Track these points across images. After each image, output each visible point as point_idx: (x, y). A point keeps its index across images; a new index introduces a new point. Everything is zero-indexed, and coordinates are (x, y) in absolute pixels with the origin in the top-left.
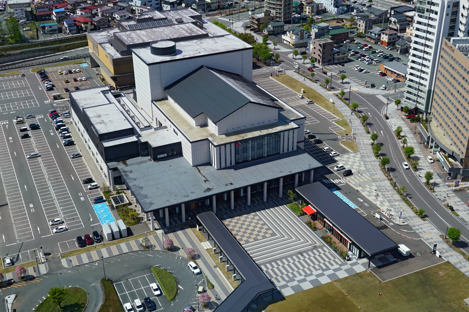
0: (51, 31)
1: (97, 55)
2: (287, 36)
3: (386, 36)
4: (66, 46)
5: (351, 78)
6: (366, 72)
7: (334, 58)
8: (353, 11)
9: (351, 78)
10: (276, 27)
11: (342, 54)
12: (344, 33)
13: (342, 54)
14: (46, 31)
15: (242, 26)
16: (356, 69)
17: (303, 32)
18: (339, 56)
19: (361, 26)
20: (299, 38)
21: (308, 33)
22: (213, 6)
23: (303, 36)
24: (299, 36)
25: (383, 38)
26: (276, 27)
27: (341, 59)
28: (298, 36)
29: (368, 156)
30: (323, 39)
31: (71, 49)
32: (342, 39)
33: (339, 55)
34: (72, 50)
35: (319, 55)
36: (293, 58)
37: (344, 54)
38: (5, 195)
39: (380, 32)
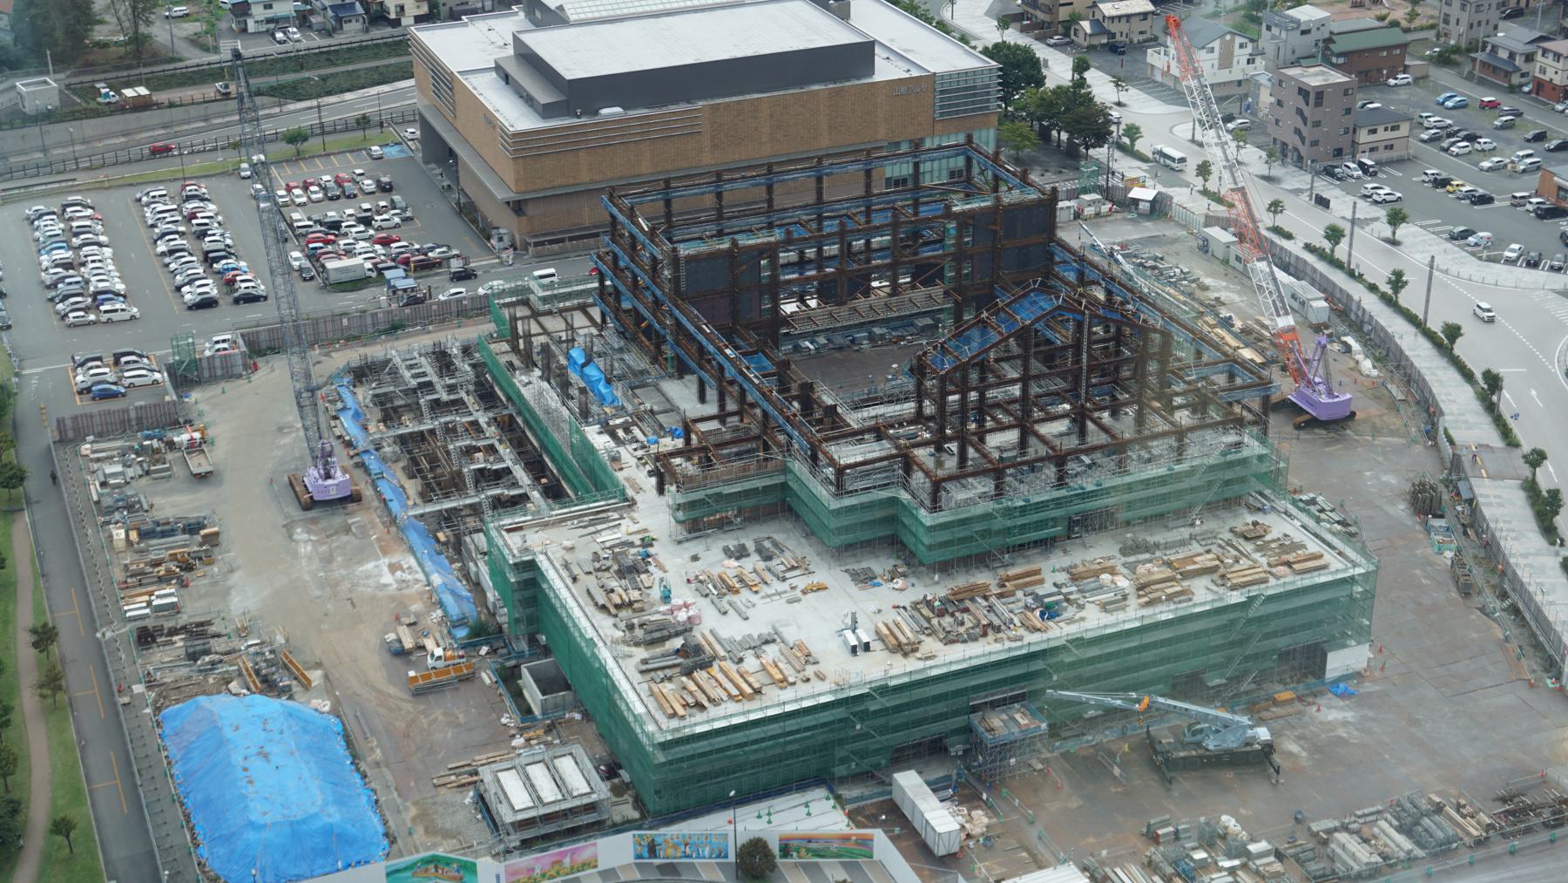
0: (269, 21)
1: (450, 115)
2: (1166, 54)
3: (1555, 64)
4: (324, 79)
5: (1424, 223)
6: (1388, 198)
7: (1354, 143)
8: (868, 291)
9: (1424, 223)
10: (1123, 20)
11: (1386, 129)
12: (1389, 48)
13: (1386, 129)
14: (251, 27)
15: (988, 13)
16: (397, 198)
17: (1233, 41)
18: (1373, 138)
19: (1453, 21)
20: (1216, 63)
21: (1250, 46)
22: (920, 12)
23: (1231, 55)
24: (1216, 54)
25: (1543, 71)
26: (1123, 20)
27: (1381, 148)
28: (1210, 55)
29: (1513, 531)
30: (1311, 70)
31: (342, 91)
32: (1379, 71)
33: (1374, 131)
34: (348, 96)
35: (1298, 132)
36: (1193, 141)
37: (1393, 129)
38: (997, 207)
39: (1530, 49)
